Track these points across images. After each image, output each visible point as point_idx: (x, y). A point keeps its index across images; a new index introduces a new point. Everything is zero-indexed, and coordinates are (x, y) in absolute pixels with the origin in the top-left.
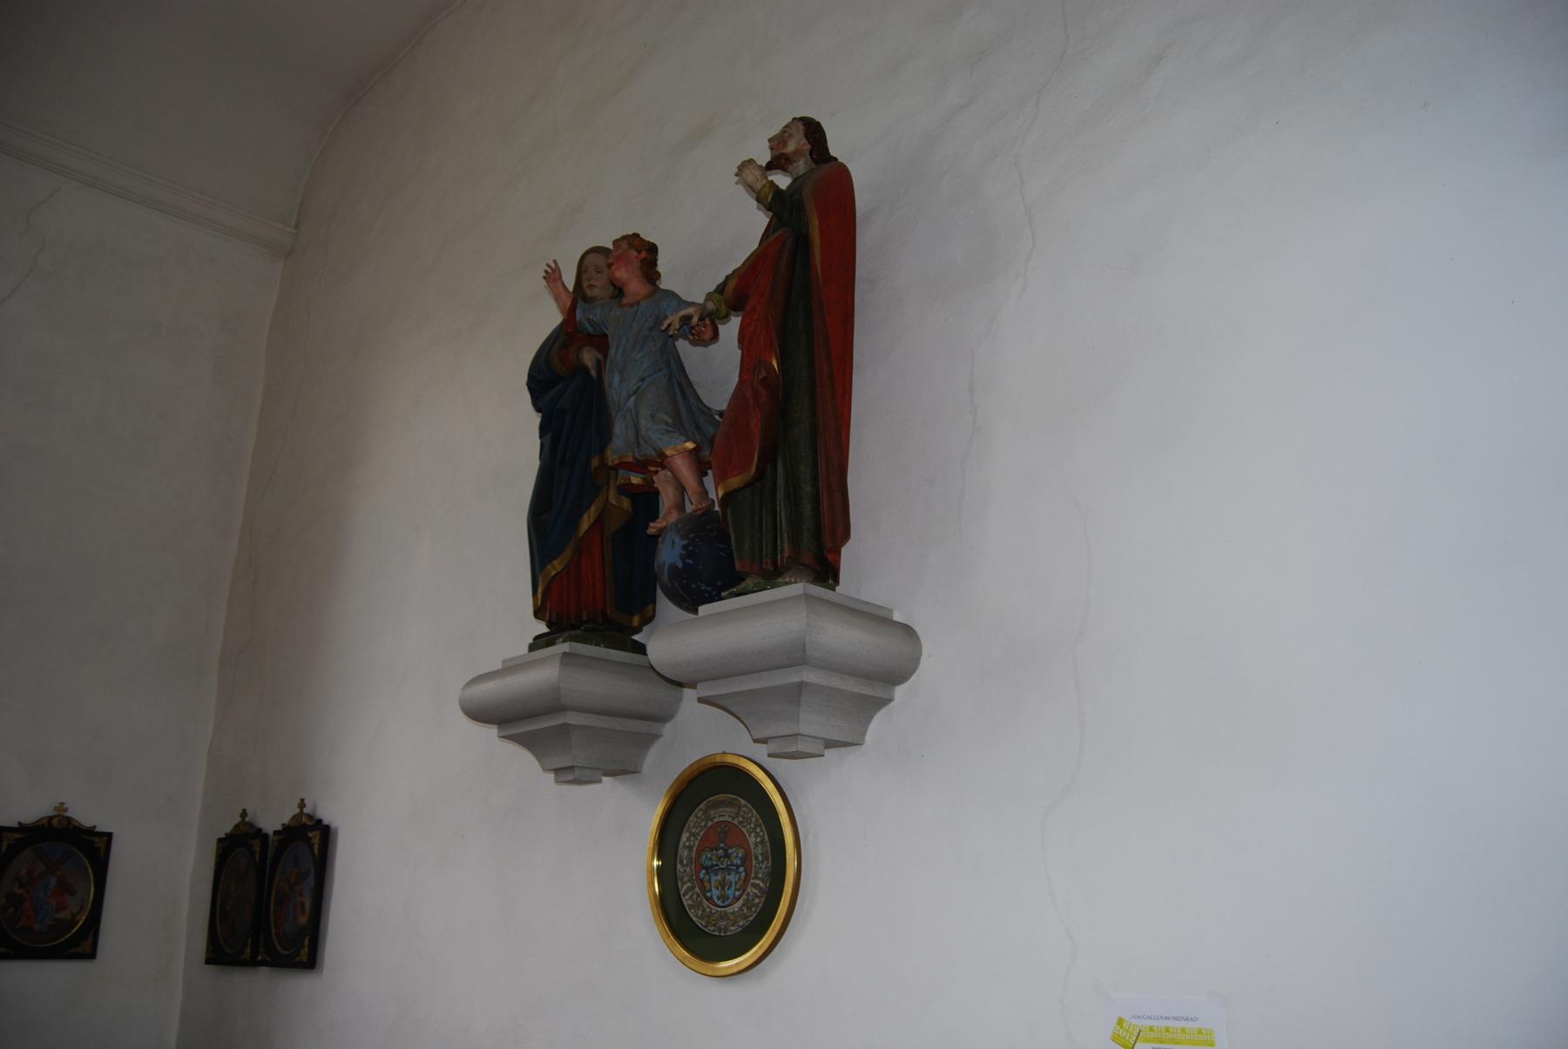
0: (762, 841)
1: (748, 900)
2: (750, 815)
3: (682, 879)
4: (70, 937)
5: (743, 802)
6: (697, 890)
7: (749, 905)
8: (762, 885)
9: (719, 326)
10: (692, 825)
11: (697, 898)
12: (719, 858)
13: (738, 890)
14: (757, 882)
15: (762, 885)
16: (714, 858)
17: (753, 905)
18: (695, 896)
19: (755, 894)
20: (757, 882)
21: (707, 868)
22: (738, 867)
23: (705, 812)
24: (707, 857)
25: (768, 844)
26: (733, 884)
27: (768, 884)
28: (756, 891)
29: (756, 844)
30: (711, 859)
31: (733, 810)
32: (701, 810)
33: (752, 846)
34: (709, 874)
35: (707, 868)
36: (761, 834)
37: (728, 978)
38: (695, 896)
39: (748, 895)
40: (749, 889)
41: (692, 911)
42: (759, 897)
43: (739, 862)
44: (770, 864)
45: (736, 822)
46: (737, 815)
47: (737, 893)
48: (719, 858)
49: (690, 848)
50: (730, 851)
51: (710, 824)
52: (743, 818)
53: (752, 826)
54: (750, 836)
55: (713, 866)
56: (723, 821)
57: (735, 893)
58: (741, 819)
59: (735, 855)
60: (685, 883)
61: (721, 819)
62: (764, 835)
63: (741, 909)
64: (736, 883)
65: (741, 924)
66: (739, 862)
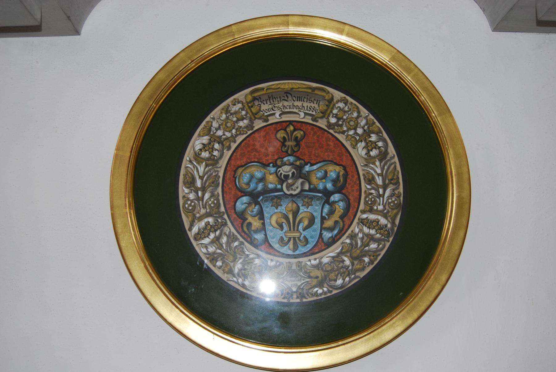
0: (383, 156)
1: (353, 246)
2: (355, 114)
3: (191, 212)
4: (345, 290)
5: (337, 94)
6: (230, 228)
7: (357, 253)
8: (383, 221)
9: (304, 189)
10: (215, 124)
11: (228, 243)
12: (282, 179)
13: (331, 229)
14: (372, 217)
15: (383, 221)
16: (271, 178)
17: (365, 254)
18: (224, 240)
19: (368, 235)
20: (372, 217)
21: (254, 197)
22: (327, 194)
23: (249, 105)
24: (252, 177)
25: (396, 159)
26: (318, 221)
27: (397, 222)
28: (373, 232)
29: (369, 160)
30: (262, 179)
31: (318, 107)
32: (237, 101)
33: (359, 163)
34: (257, 203)
35: (254, 197)
36: (380, 144)
37: (338, 22)
38: (224, 240)
39: (353, 237)
40: (355, 228)
41: (219, 264)
42: (378, 241)
43: (329, 186)
44: (401, 189)
45: (322, 124)
46: (325, 114)
47: (327, 235)
48: (282, 179)
49: (213, 162)
50: (307, 168)
51: (259, 124)
52: (339, 119)
53: (360, 131)
54: (354, 147)
55: (266, 191)
56: (291, 122)
57: (321, 234)
58: (333, 120)
59: (320, 174)
60: (201, 219)
61: (285, 118)
62: (386, 146)
63: (336, 259)
64: (323, 219)
65: (339, 282)
66: (329, 186)
